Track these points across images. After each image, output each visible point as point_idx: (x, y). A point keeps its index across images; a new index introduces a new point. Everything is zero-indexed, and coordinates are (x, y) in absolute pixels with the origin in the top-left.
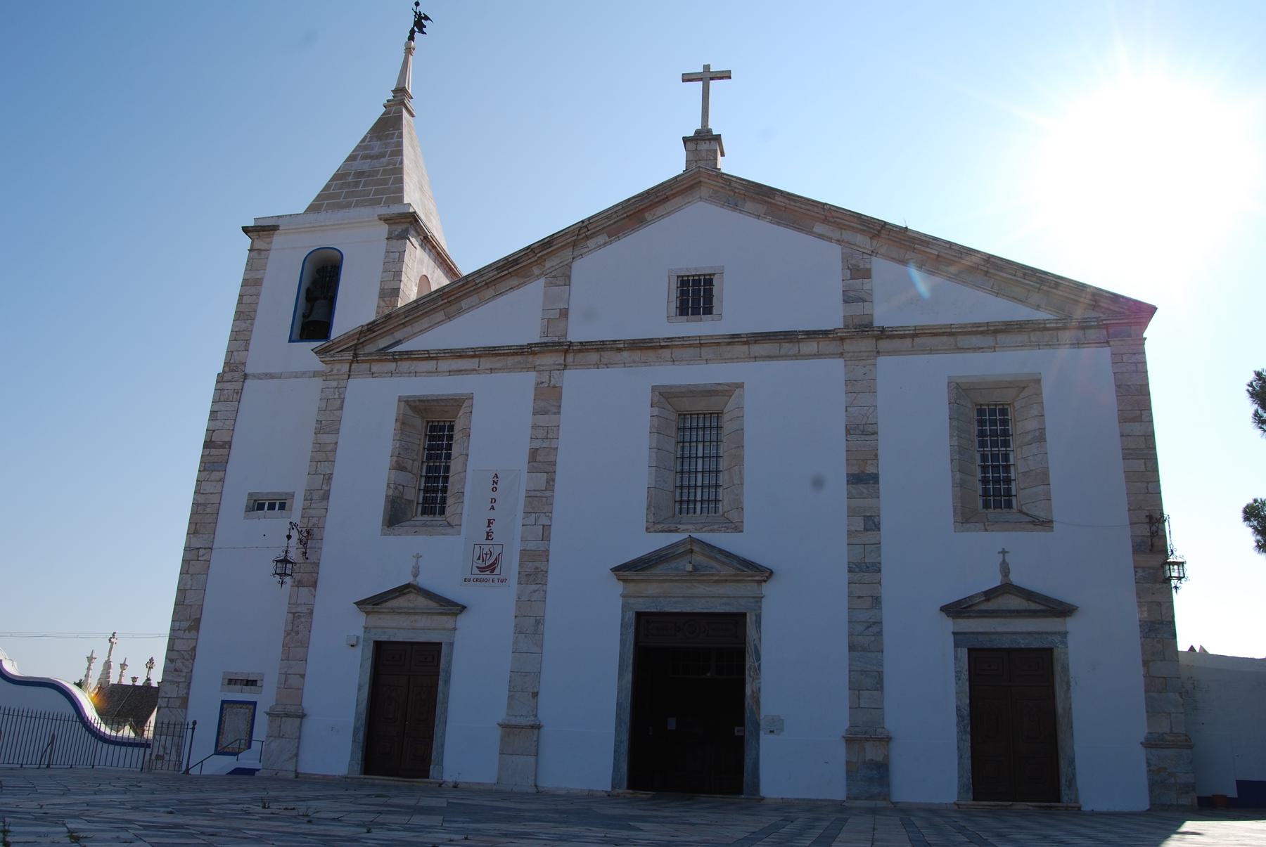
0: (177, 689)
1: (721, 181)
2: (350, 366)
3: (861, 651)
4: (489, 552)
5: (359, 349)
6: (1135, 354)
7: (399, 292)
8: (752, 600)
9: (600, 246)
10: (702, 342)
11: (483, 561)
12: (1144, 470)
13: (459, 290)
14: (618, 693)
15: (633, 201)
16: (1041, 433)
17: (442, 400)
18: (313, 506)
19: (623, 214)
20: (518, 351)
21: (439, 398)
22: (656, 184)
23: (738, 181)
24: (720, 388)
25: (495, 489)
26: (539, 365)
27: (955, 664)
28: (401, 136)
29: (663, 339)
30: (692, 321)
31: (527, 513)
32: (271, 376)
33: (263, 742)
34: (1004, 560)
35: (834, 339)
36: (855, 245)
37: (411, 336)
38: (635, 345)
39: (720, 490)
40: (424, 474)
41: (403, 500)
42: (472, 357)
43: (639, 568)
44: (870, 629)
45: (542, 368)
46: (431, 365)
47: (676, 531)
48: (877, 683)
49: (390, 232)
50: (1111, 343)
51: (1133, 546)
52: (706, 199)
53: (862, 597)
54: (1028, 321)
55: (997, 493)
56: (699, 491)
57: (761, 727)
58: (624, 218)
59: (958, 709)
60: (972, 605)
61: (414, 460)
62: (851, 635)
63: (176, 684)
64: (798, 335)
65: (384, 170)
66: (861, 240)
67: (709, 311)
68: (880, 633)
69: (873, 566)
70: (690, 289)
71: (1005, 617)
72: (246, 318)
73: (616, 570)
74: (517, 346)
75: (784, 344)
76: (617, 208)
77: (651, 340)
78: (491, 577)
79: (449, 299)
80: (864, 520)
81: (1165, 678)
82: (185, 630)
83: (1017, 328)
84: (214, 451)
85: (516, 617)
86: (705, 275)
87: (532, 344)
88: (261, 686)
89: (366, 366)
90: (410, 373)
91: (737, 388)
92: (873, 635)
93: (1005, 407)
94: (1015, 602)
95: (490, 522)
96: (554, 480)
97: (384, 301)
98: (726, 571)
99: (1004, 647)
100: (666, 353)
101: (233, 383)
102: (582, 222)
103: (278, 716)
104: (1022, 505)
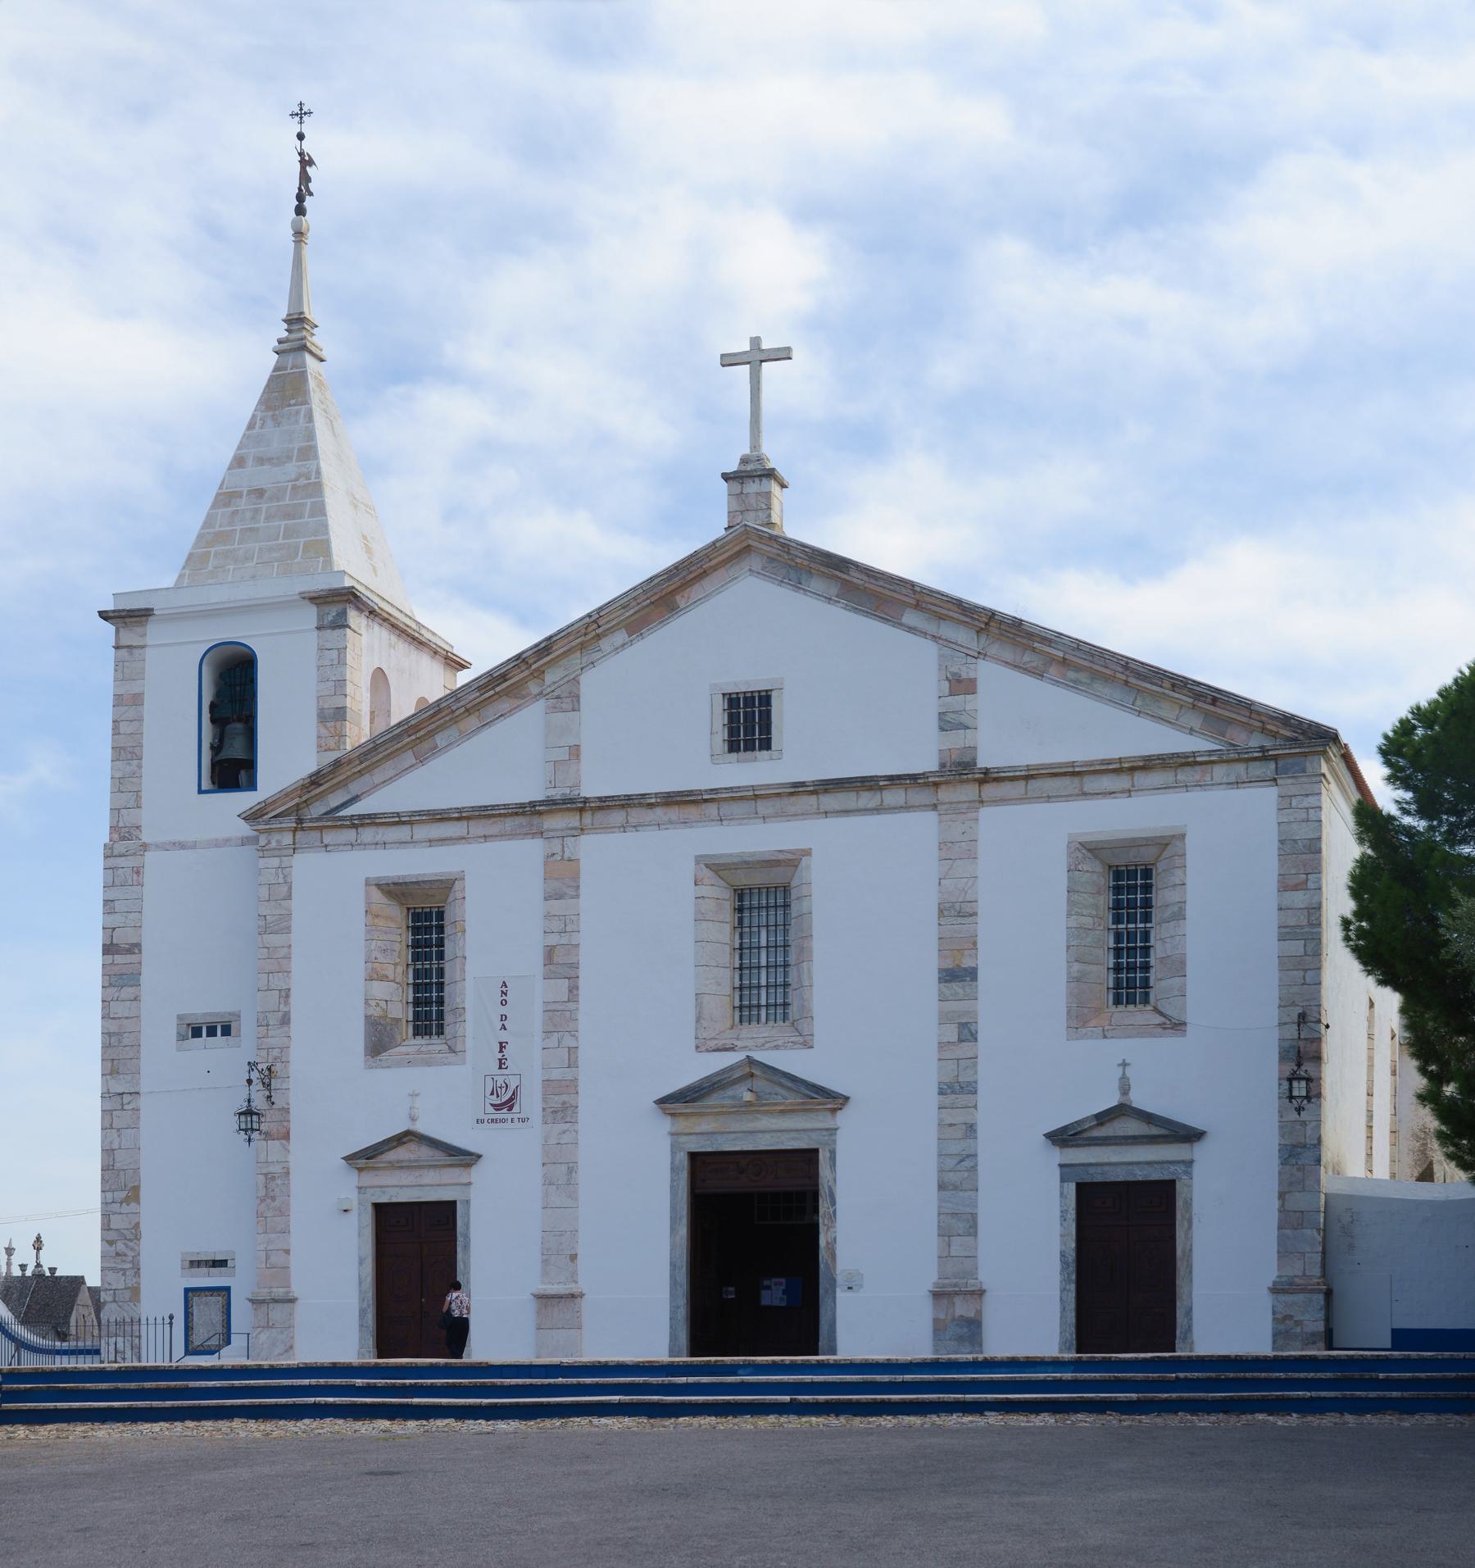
0: (123, 1278)
1: (776, 546)
2: (294, 836)
3: (952, 1190)
4: (504, 1085)
5: (302, 808)
6: (1307, 795)
7: (345, 712)
8: (825, 1133)
9: (617, 649)
10: (756, 793)
11: (498, 1096)
12: (1303, 954)
13: (429, 722)
14: (671, 1250)
15: (656, 581)
16: (1180, 907)
17: (424, 882)
18: (271, 1033)
19: (644, 601)
20: (517, 810)
21: (420, 879)
22: (683, 557)
23: (799, 547)
24: (781, 857)
25: (504, 1003)
26: (548, 830)
27: (1061, 1202)
28: (310, 418)
29: (706, 791)
30: (745, 761)
31: (547, 1033)
32: (182, 846)
33: (248, 1334)
34: (1124, 1073)
35: (926, 784)
36: (955, 643)
37: (371, 789)
38: (670, 799)
39: (789, 990)
40: (411, 981)
41: (388, 1020)
42: (458, 819)
43: (688, 1099)
44: (963, 1163)
45: (551, 834)
46: (402, 833)
47: (732, 1049)
48: (970, 1227)
49: (320, 617)
50: (1279, 781)
51: (1279, 1053)
52: (759, 573)
53: (955, 1125)
54: (1173, 754)
55: (1131, 984)
56: (763, 992)
57: (838, 1284)
58: (647, 606)
59: (1063, 1254)
60: (1085, 1130)
61: (395, 965)
62: (941, 1171)
63: (121, 1273)
64: (879, 781)
65: (294, 488)
66: (964, 636)
67: (766, 745)
68: (974, 1168)
69: (967, 1086)
70: (742, 711)
71: (1121, 1144)
72: (129, 757)
73: (661, 1102)
74: (516, 804)
75: (861, 792)
76: (637, 592)
77: (690, 793)
78: (509, 1116)
79: (418, 735)
80: (959, 1028)
81: (1302, 1212)
82: (121, 1203)
83: (1160, 764)
84: (119, 959)
85: (543, 1164)
86: (759, 692)
87: (535, 802)
88: (234, 1267)
89: (315, 835)
90: (377, 844)
91: (803, 856)
92: (966, 1171)
93: (1149, 867)
94: (1132, 1127)
95: (502, 1046)
96: (577, 988)
97: (326, 727)
98: (793, 1099)
99: (1119, 1180)
100: (712, 809)
101: (129, 858)
102: (589, 615)
103: (263, 1302)
104: (1157, 1000)
